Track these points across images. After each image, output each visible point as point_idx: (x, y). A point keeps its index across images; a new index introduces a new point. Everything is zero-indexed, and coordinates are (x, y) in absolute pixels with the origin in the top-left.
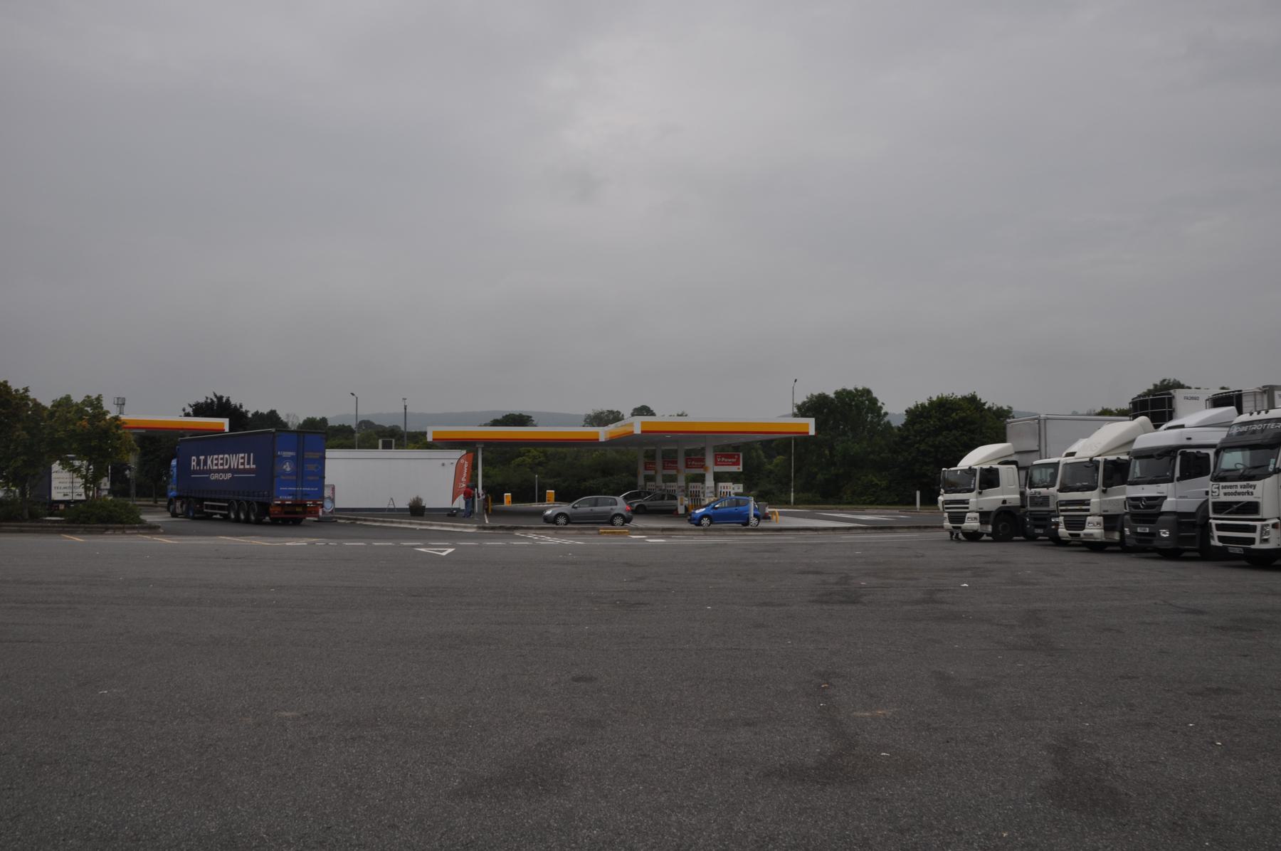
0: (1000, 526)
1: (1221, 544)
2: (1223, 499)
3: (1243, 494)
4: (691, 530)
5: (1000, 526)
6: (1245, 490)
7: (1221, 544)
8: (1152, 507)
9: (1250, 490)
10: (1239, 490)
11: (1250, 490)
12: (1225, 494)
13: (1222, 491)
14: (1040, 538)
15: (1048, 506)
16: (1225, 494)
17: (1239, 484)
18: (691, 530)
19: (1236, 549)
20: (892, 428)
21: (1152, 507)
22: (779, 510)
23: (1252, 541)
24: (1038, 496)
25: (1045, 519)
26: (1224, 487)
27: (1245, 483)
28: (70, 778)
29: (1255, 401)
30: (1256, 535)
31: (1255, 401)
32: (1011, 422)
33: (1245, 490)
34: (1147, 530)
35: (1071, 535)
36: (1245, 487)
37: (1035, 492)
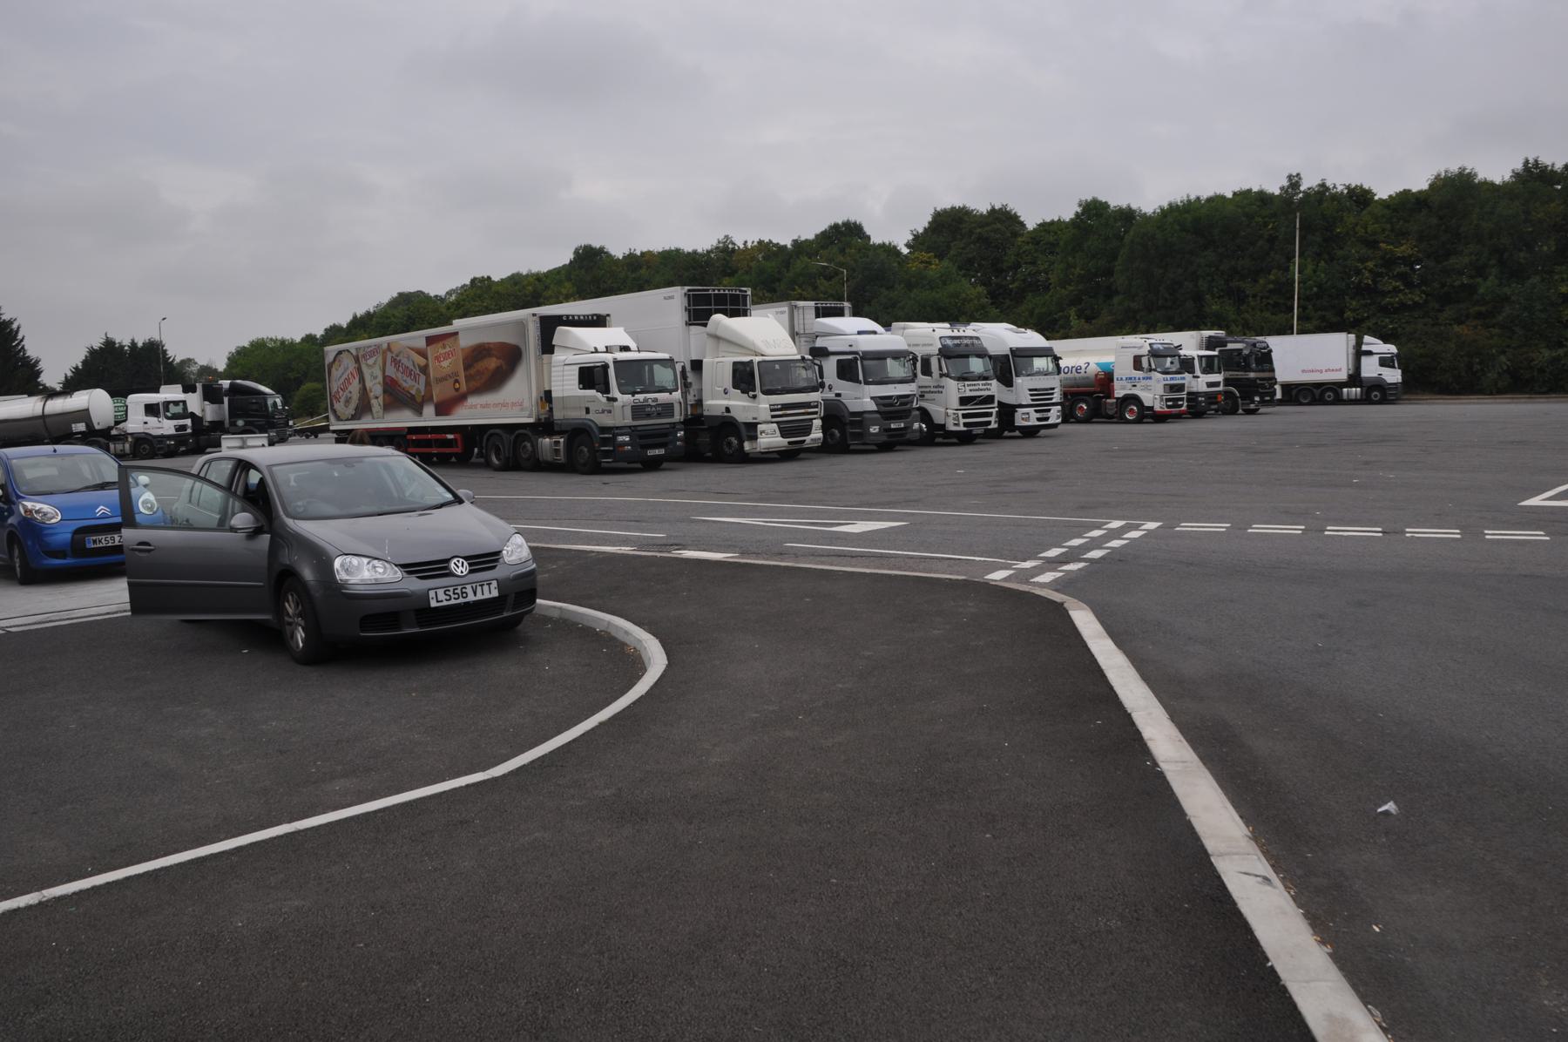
0: (1135, 408)
1: (965, 429)
2: (969, 394)
3: (985, 390)
4: (11, 627)
5: (1135, 408)
6: (985, 387)
7: (965, 429)
8: (906, 404)
9: (989, 387)
10: (981, 387)
11: (989, 387)
12: (971, 390)
13: (968, 388)
14: (1184, 416)
15: (672, 416)
16: (971, 390)
17: (980, 382)
18: (11, 627)
19: (978, 430)
20: (431, 297)
21: (906, 404)
22: (562, 450)
23: (989, 423)
24: (654, 404)
25: (666, 435)
26: (968, 385)
27: (984, 382)
28: (1273, 220)
29: (804, 324)
30: (962, 421)
31: (804, 324)
32: (914, 328)
33: (985, 387)
34: (902, 425)
35: (789, 443)
36: (985, 385)
37: (646, 400)
